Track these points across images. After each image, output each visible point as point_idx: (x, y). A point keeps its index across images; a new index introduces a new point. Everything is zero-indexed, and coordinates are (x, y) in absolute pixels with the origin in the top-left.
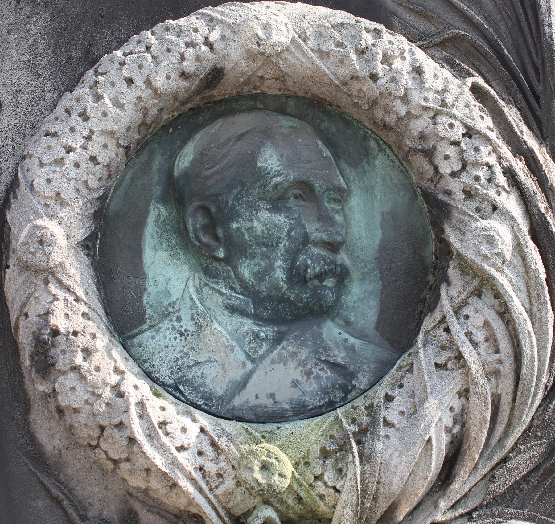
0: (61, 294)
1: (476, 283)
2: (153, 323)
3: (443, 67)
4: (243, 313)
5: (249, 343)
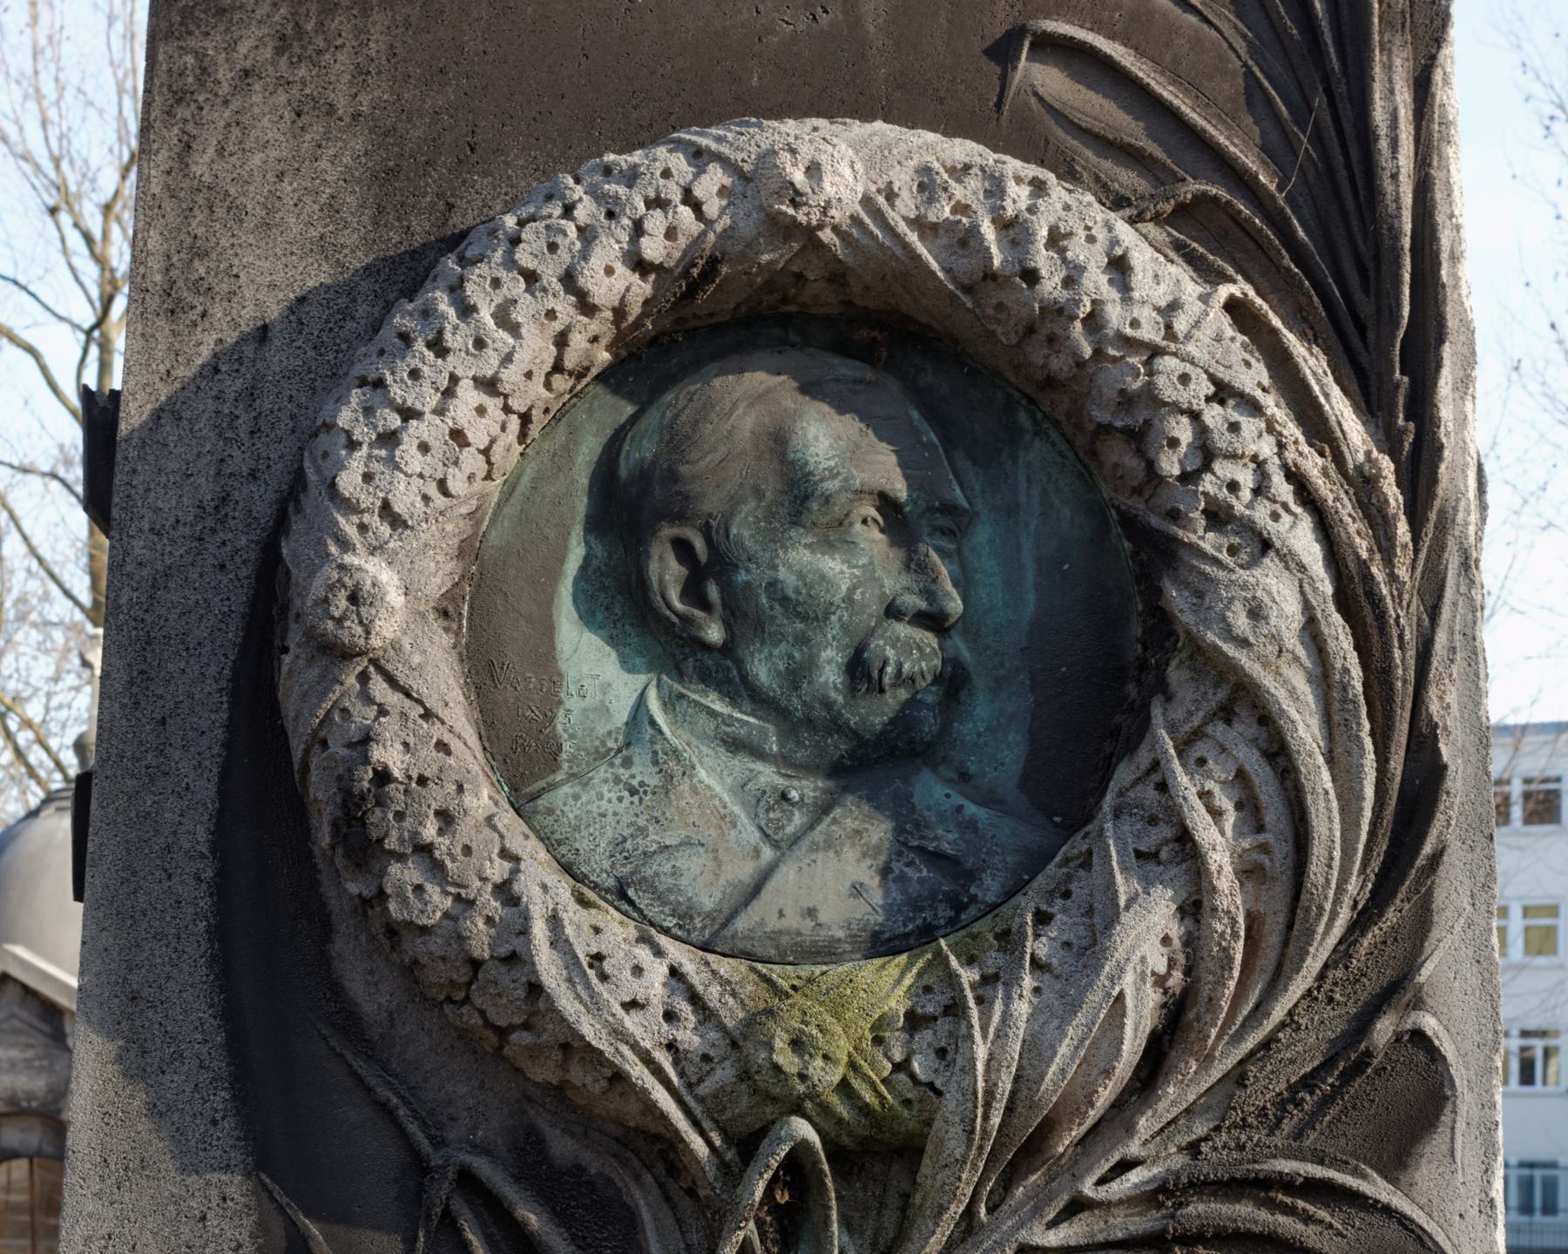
0: (392, 699)
1: (1222, 694)
2: (575, 770)
3: (1172, 261)
4: (758, 753)
5: (768, 811)
